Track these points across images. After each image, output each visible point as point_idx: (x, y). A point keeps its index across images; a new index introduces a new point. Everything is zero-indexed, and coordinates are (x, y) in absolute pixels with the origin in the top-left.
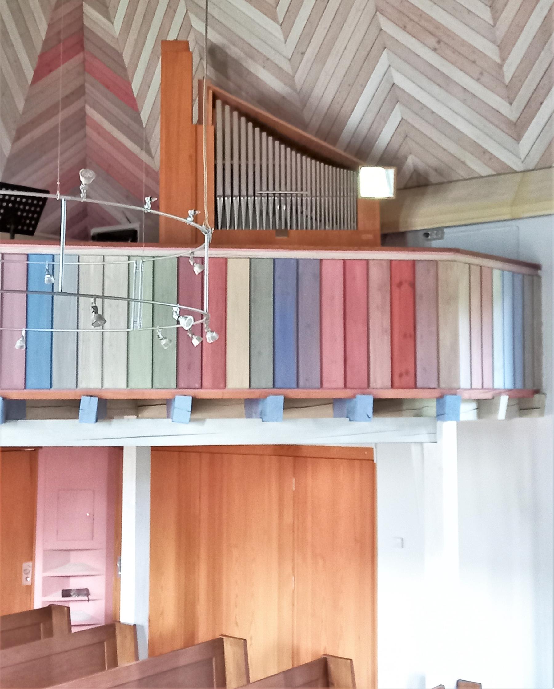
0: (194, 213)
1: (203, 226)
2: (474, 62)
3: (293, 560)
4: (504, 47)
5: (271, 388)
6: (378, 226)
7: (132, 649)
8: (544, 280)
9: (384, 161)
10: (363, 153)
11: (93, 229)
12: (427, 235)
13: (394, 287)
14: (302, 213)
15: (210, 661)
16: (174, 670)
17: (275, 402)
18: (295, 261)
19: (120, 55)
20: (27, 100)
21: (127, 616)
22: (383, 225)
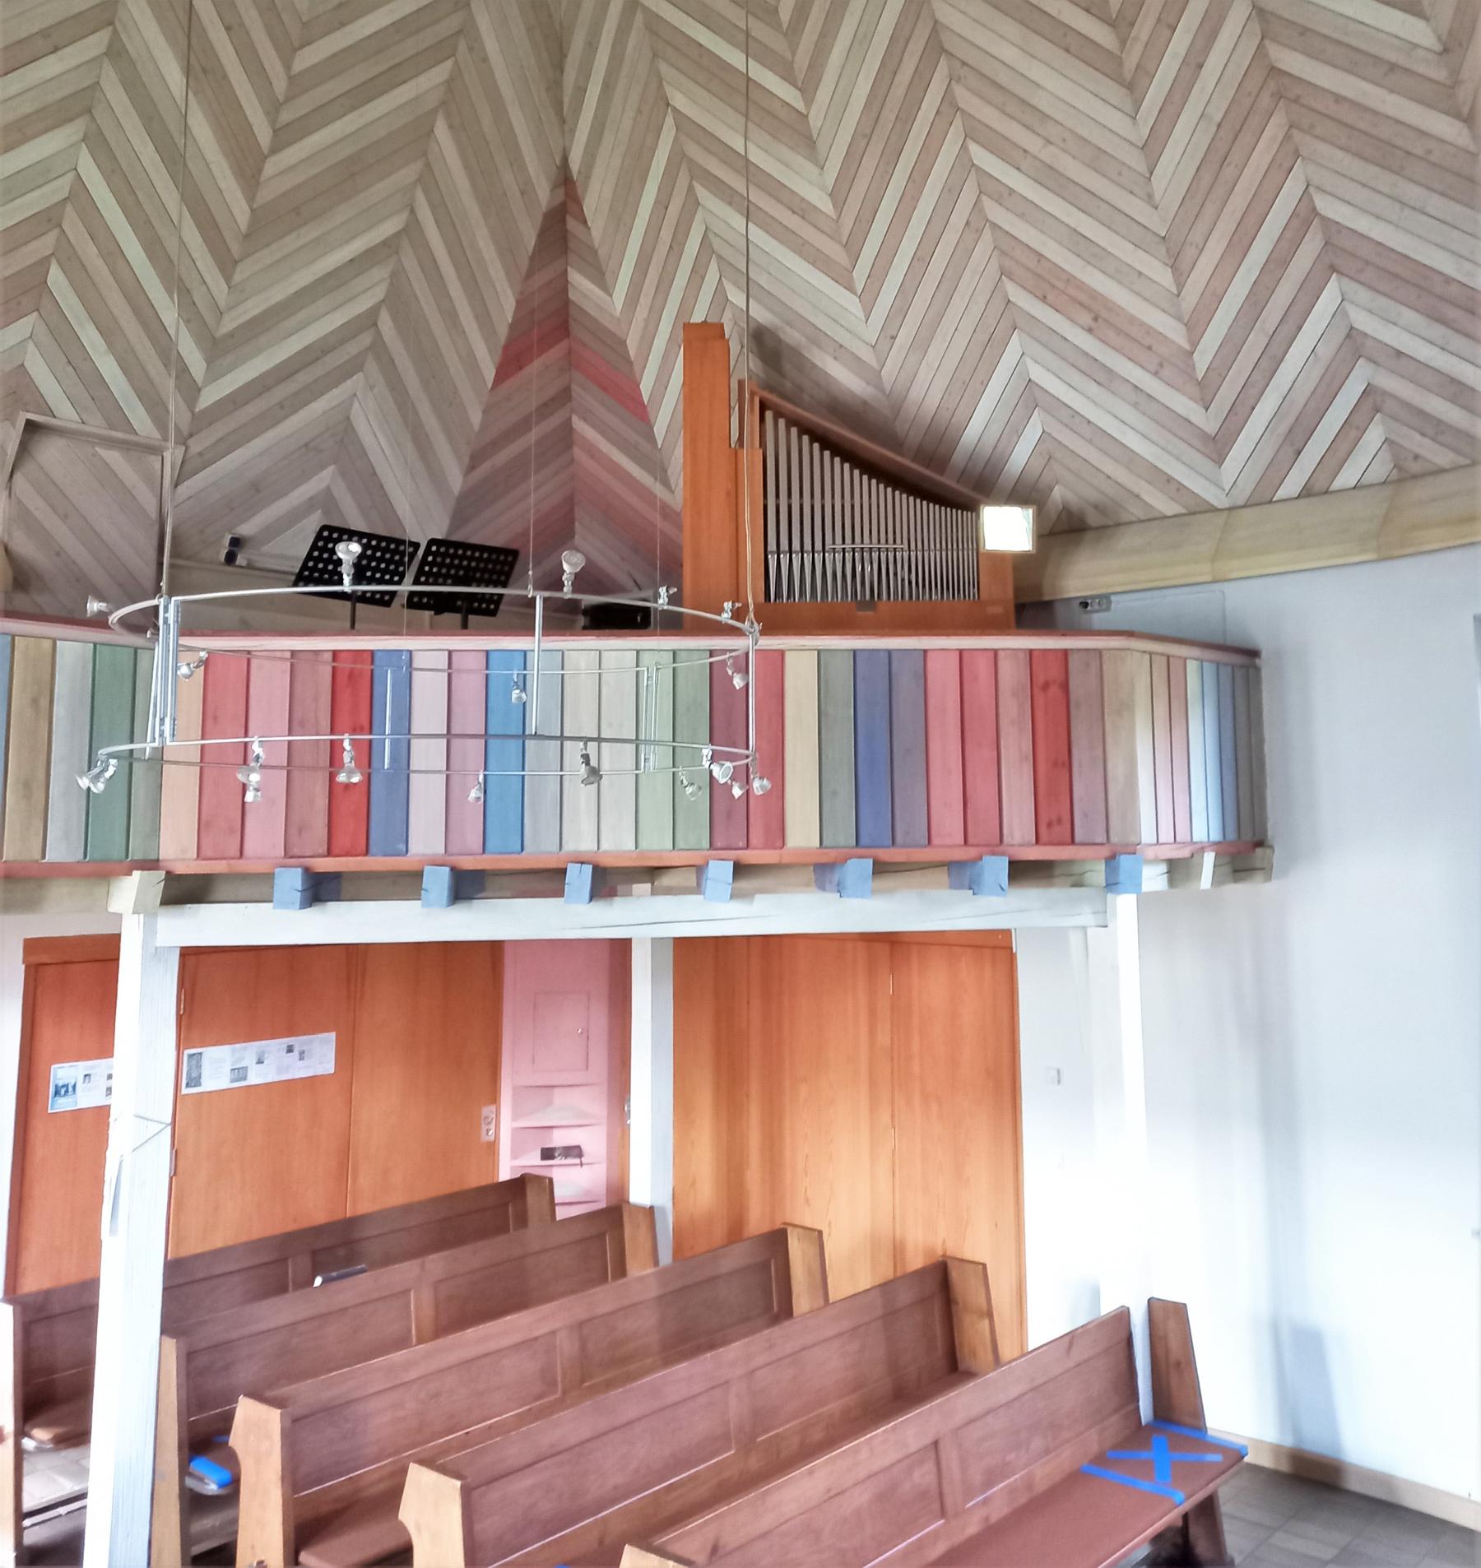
3: (893, 1103)
4: (1195, 326)
6: (1010, 594)
7: (648, 1246)
8: (1265, 673)
9: (1017, 496)
12: (1085, 605)
13: (1036, 691)
14: (895, 574)
15: (765, 1266)
16: (713, 1279)
19: (623, 343)
21: (640, 1194)
22: (1018, 590)
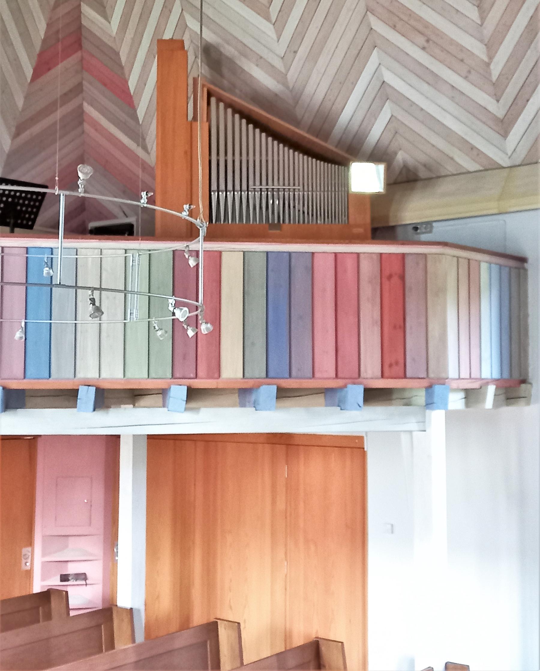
0: (189, 208)
1: (198, 220)
2: (462, 60)
3: (286, 545)
4: (492, 46)
5: (264, 378)
6: (368, 220)
7: (129, 632)
8: (530, 273)
9: (374, 157)
10: (353, 149)
11: (90, 223)
12: (416, 229)
13: (384, 280)
14: (294, 207)
15: (204, 644)
16: (170, 652)
17: (268, 391)
18: (288, 254)
19: (117, 54)
20: (26, 98)
21: (124, 600)
22: (373, 220)
